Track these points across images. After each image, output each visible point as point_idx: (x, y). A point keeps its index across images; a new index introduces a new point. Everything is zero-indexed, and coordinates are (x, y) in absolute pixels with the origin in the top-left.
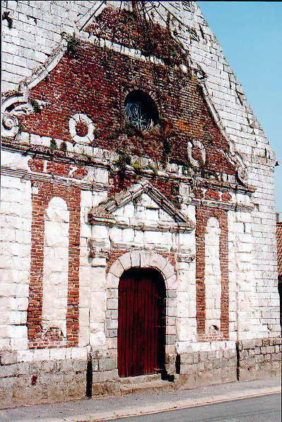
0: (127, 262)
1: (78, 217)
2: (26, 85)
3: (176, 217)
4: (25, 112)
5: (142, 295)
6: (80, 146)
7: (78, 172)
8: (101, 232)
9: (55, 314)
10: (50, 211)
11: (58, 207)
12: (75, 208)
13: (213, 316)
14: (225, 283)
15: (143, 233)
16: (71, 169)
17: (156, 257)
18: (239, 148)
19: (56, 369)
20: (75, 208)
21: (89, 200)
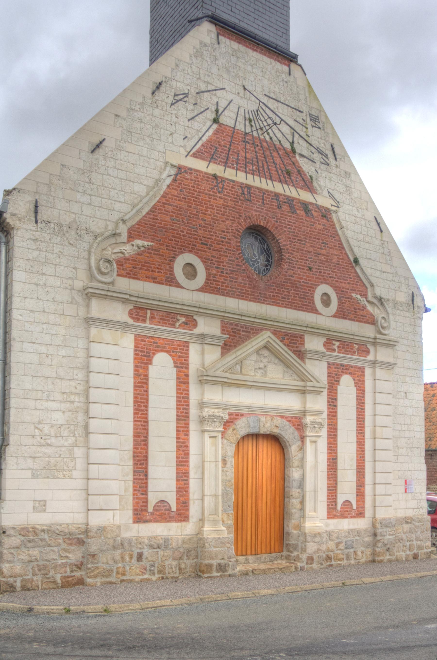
0: (243, 427)
1: (187, 376)
2: (124, 221)
3: (303, 377)
4: (123, 253)
5: (406, 546)
6: (187, 294)
7: (185, 323)
8: (214, 395)
9: (162, 484)
10: (153, 371)
11: (162, 366)
12: (182, 365)
13: (346, 491)
14: (289, 324)
15: (268, 397)
16: (178, 320)
17: (278, 421)
18: (379, 292)
19: (164, 544)
20: (182, 365)
21: (199, 357)
